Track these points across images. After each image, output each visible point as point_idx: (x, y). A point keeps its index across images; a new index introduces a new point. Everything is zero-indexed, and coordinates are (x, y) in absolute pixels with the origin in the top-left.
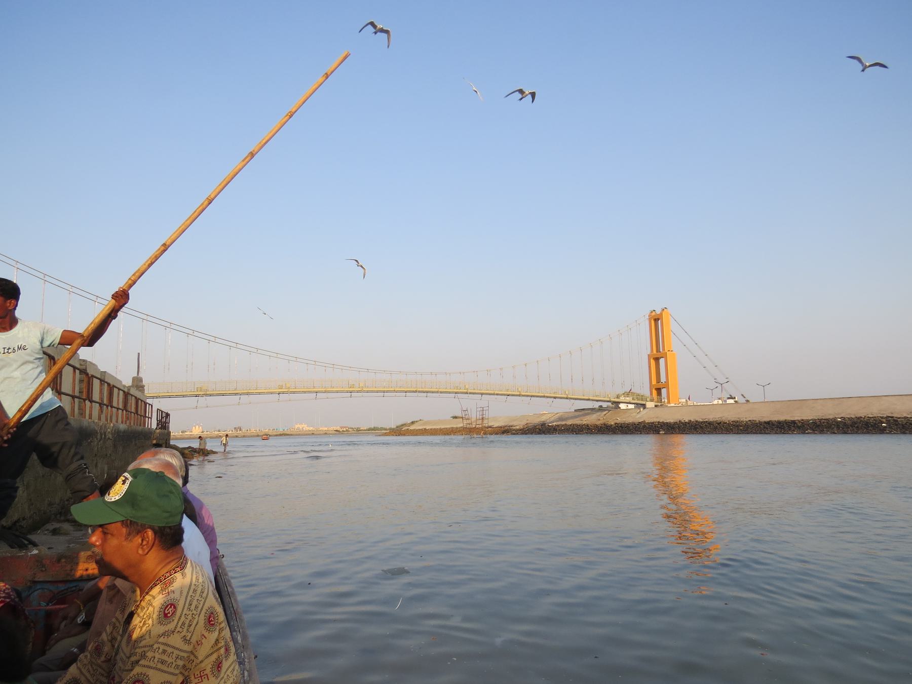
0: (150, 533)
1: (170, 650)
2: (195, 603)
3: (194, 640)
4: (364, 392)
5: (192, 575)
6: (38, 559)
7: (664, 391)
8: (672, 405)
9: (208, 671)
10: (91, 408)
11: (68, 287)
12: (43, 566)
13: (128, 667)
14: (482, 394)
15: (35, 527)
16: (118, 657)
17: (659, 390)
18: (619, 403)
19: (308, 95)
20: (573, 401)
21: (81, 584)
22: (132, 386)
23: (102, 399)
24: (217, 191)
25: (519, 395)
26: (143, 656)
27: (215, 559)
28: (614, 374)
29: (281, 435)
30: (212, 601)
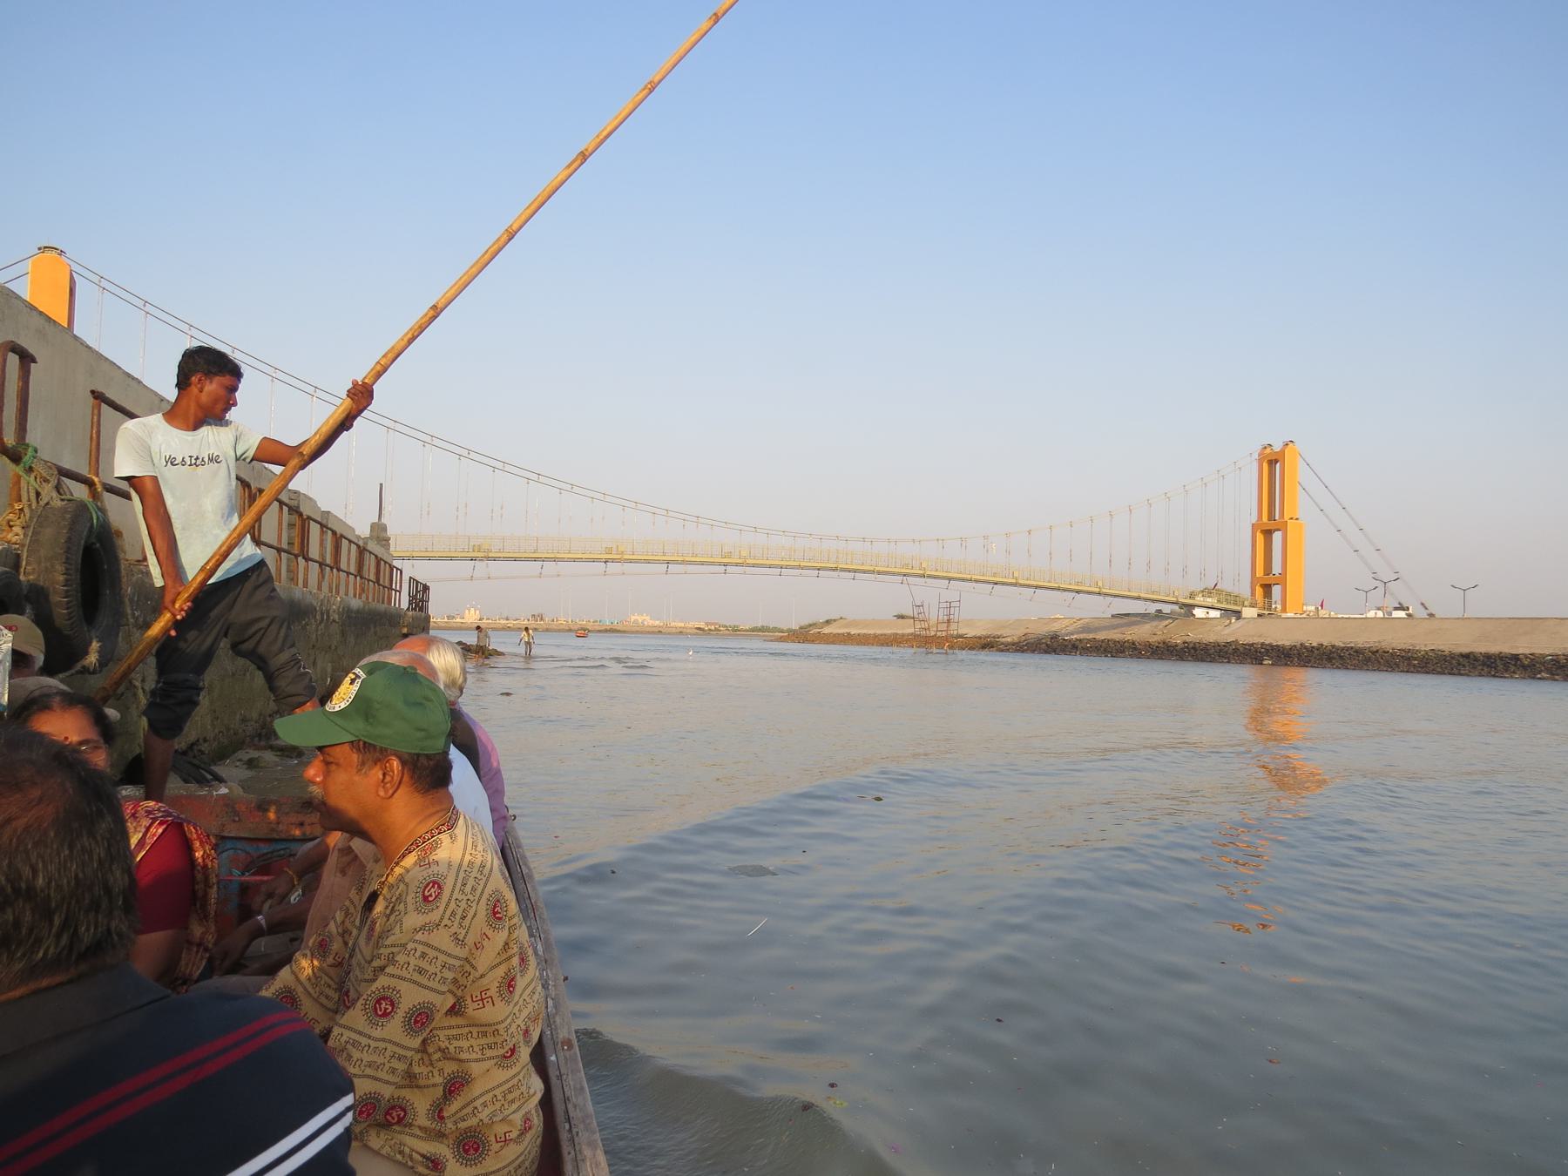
0: (395, 763)
1: (432, 953)
2: (471, 883)
3: (470, 940)
4: (749, 565)
5: (463, 846)
6: (228, 803)
7: (1276, 590)
8: (1290, 615)
9: (493, 992)
10: (307, 569)
11: (270, 370)
12: (236, 813)
13: (369, 975)
14: (950, 579)
15: (222, 755)
16: (354, 961)
17: (1267, 588)
18: (1194, 606)
19: (682, 51)
20: (1109, 599)
21: (293, 846)
22: (371, 538)
23: (323, 555)
24: (524, 218)
25: (1015, 585)
26: (391, 960)
27: (501, 818)
28: (1191, 552)
29: (606, 631)
30: (498, 881)
